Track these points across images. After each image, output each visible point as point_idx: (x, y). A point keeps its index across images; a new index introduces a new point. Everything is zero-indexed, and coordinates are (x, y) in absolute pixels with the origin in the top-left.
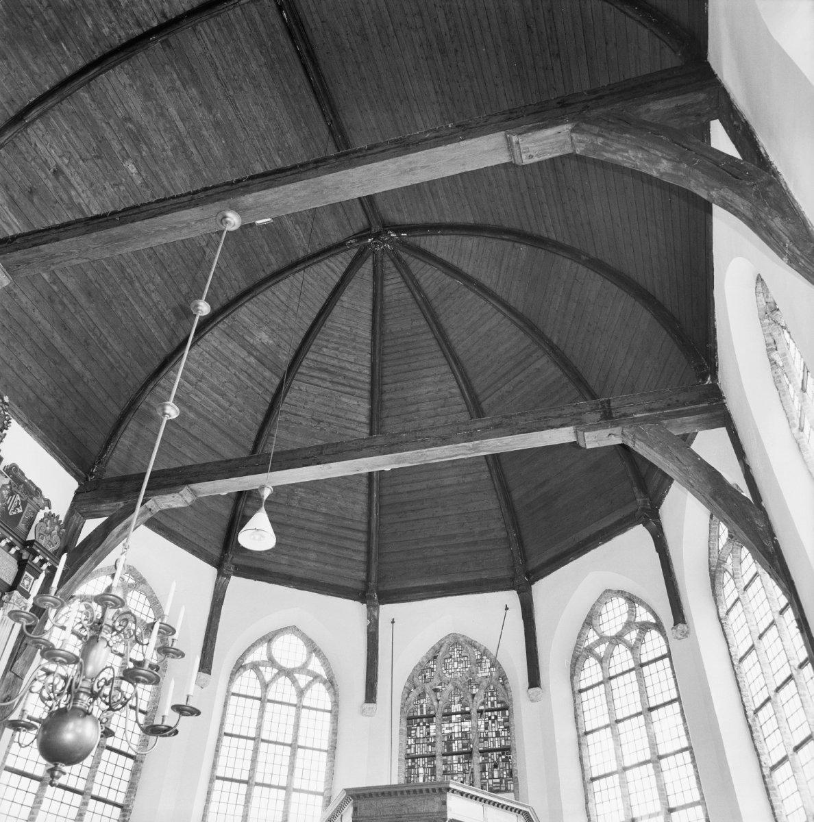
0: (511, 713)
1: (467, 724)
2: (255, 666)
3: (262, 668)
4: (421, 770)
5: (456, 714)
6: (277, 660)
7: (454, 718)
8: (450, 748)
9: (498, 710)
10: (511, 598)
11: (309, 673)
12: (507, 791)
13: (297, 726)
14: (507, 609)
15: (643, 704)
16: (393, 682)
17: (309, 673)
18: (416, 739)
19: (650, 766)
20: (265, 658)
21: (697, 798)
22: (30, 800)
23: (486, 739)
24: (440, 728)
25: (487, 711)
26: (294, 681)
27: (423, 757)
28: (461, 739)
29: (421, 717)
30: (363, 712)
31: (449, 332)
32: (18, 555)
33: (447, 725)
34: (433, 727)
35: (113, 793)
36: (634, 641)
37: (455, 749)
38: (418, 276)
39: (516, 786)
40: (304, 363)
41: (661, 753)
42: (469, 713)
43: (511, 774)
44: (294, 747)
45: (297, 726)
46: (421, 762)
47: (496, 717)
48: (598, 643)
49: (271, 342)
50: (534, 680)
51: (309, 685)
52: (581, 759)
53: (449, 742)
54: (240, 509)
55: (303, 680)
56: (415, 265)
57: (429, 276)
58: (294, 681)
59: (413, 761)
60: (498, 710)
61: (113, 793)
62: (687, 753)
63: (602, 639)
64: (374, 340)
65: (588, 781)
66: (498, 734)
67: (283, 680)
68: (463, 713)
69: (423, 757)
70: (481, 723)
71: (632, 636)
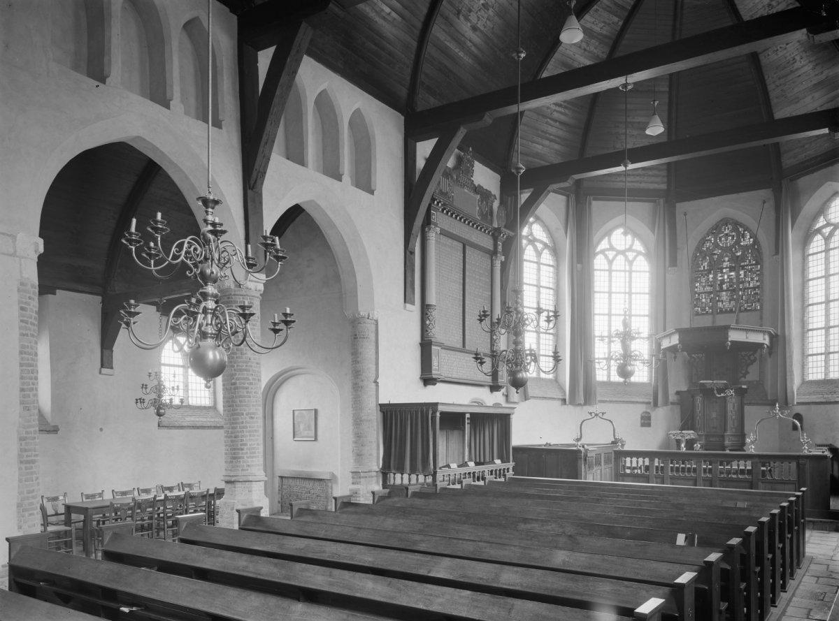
2: (603, 252)
3: (607, 253)
6: (615, 246)
7: (724, 271)
14: (764, 202)
17: (634, 251)
22: (638, 296)
26: (626, 257)
28: (729, 282)
32: (493, 235)
35: (815, 360)
36: (827, 234)
44: (610, 293)
51: (635, 258)
59: (699, 295)
61: (815, 360)
66: (752, 279)
67: (620, 258)
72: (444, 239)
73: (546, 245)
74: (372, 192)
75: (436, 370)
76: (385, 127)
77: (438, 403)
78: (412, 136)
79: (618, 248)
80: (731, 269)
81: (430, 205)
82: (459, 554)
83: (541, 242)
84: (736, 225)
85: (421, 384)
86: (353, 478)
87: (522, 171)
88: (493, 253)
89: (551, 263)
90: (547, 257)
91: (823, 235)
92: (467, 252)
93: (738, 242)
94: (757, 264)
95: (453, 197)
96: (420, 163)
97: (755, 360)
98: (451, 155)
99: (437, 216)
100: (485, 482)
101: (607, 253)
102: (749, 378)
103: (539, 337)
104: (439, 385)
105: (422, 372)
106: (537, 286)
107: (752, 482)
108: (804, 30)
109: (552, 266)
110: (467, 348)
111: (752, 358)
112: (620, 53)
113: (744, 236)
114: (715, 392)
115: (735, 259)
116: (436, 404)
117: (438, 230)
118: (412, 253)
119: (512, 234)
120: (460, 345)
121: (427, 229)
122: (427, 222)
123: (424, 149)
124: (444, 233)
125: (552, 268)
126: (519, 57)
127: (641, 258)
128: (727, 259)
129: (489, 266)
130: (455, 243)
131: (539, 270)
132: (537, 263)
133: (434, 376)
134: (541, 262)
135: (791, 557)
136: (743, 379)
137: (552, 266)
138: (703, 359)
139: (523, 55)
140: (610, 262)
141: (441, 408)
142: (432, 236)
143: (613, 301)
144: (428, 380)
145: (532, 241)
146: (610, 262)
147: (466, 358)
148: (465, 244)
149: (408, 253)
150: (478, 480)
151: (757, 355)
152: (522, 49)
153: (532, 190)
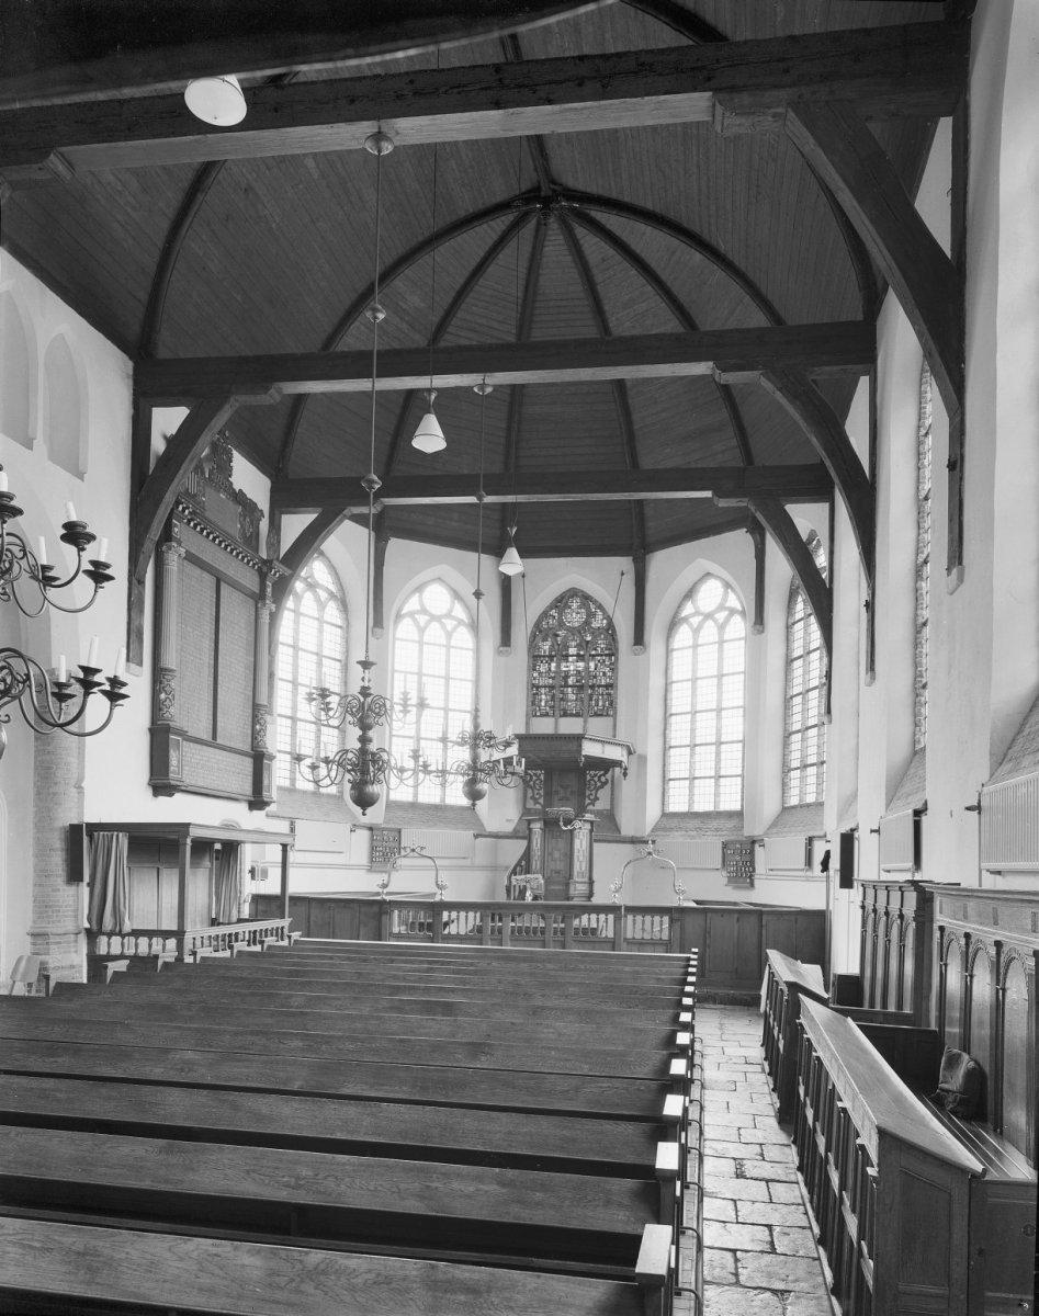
0: (617, 659)
1: (581, 664)
2: (411, 614)
3: (416, 616)
4: (543, 697)
5: (572, 656)
7: (570, 659)
8: (566, 682)
9: (606, 655)
10: (625, 563)
11: (454, 618)
12: (607, 715)
13: (448, 662)
14: (623, 574)
15: (716, 771)
16: (521, 634)
17: (454, 618)
18: (540, 673)
19: (713, 780)
20: (419, 608)
21: (740, 773)
23: (595, 677)
24: (558, 666)
25: (598, 655)
27: (545, 687)
29: (544, 656)
30: (500, 653)
31: (605, 302)
33: (564, 664)
34: (553, 665)
37: (570, 683)
38: (582, 242)
39: (615, 713)
40: (459, 315)
41: (722, 740)
42: (583, 656)
43: (611, 704)
45: (448, 662)
46: (543, 691)
47: (604, 661)
48: (693, 615)
49: (422, 305)
50: (639, 638)
51: (455, 629)
52: (666, 700)
53: (567, 677)
54: (409, 409)
55: (450, 624)
56: (581, 232)
57: (591, 244)
58: (443, 626)
60: (606, 655)
62: (741, 744)
63: (697, 613)
64: (509, 429)
65: (665, 780)
66: (604, 674)
67: (435, 625)
68: (578, 655)
69: (545, 687)
70: (592, 665)
71: (721, 616)
72: (189, 567)
73: (332, 595)
74: (80, 476)
75: (174, 772)
76: (104, 373)
77: (189, 824)
78: (146, 396)
79: (433, 612)
80: (580, 657)
81: (172, 510)
82: (125, 1088)
83: (327, 590)
84: (586, 599)
85: (150, 791)
86: (34, 944)
87: (377, 486)
88: (259, 598)
89: (340, 623)
90: (333, 612)
91: (690, 626)
92: (222, 592)
93: (587, 623)
94: (610, 655)
95: (204, 502)
96: (158, 445)
97: (606, 783)
98: (833, 488)
99: (178, 529)
100: (195, 958)
101: (416, 616)
102: (599, 806)
103: (319, 730)
104: (178, 796)
105: (151, 775)
106: (317, 654)
107: (614, 942)
108: (711, 364)
109: (340, 627)
110: (219, 741)
111: (603, 779)
112: (448, 340)
113: (594, 615)
114: (561, 824)
115: (583, 645)
116: (187, 825)
117: (182, 551)
118: (141, 582)
119: (288, 572)
120: (207, 736)
121: (164, 548)
122: (167, 536)
123: (168, 420)
124: (191, 558)
125: (339, 630)
126: (375, 318)
127: (737, 619)
128: (574, 643)
129: (253, 617)
130: (206, 576)
131: (321, 631)
132: (318, 619)
133: (172, 782)
134: (325, 618)
135: (902, 947)
136: (591, 807)
137: (340, 627)
138: (542, 777)
139: (381, 316)
140: (422, 630)
141: (194, 832)
142: (173, 561)
143: (452, 690)
144: (161, 784)
145: (312, 586)
146: (422, 630)
147: (217, 757)
148: (219, 579)
149: (135, 581)
150: (255, 944)
151: (609, 776)
152: (380, 307)
153: (320, 510)
